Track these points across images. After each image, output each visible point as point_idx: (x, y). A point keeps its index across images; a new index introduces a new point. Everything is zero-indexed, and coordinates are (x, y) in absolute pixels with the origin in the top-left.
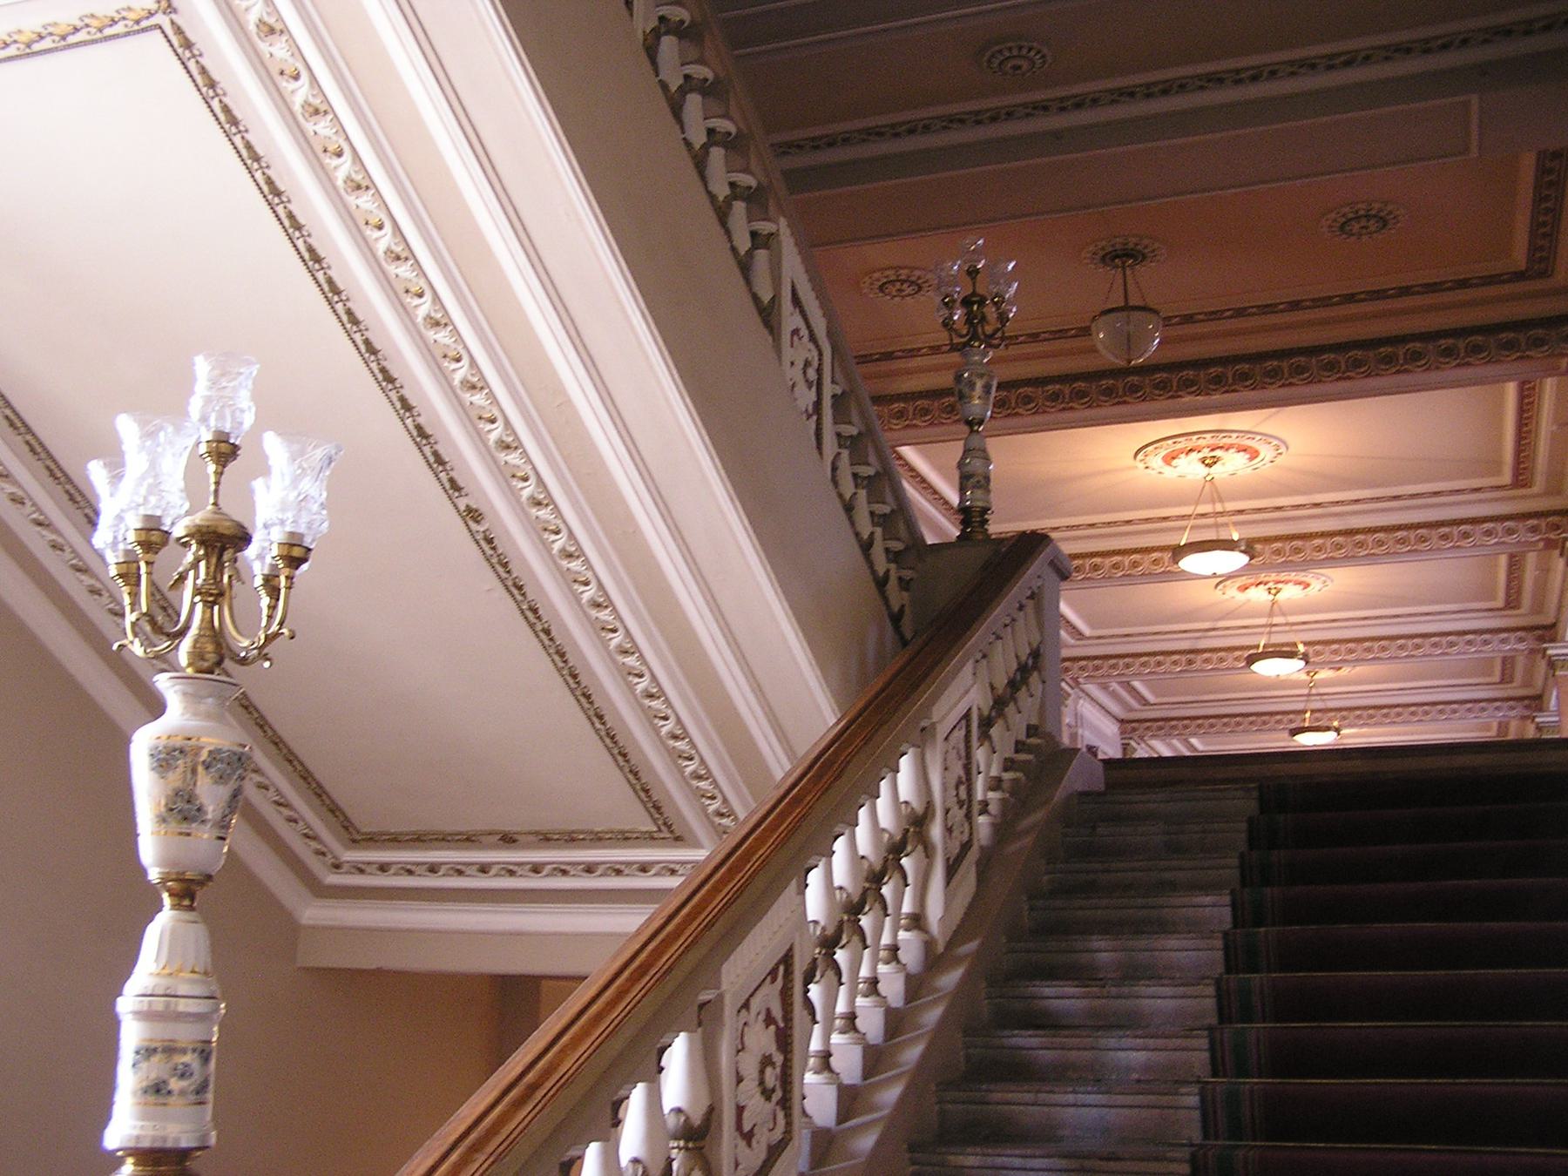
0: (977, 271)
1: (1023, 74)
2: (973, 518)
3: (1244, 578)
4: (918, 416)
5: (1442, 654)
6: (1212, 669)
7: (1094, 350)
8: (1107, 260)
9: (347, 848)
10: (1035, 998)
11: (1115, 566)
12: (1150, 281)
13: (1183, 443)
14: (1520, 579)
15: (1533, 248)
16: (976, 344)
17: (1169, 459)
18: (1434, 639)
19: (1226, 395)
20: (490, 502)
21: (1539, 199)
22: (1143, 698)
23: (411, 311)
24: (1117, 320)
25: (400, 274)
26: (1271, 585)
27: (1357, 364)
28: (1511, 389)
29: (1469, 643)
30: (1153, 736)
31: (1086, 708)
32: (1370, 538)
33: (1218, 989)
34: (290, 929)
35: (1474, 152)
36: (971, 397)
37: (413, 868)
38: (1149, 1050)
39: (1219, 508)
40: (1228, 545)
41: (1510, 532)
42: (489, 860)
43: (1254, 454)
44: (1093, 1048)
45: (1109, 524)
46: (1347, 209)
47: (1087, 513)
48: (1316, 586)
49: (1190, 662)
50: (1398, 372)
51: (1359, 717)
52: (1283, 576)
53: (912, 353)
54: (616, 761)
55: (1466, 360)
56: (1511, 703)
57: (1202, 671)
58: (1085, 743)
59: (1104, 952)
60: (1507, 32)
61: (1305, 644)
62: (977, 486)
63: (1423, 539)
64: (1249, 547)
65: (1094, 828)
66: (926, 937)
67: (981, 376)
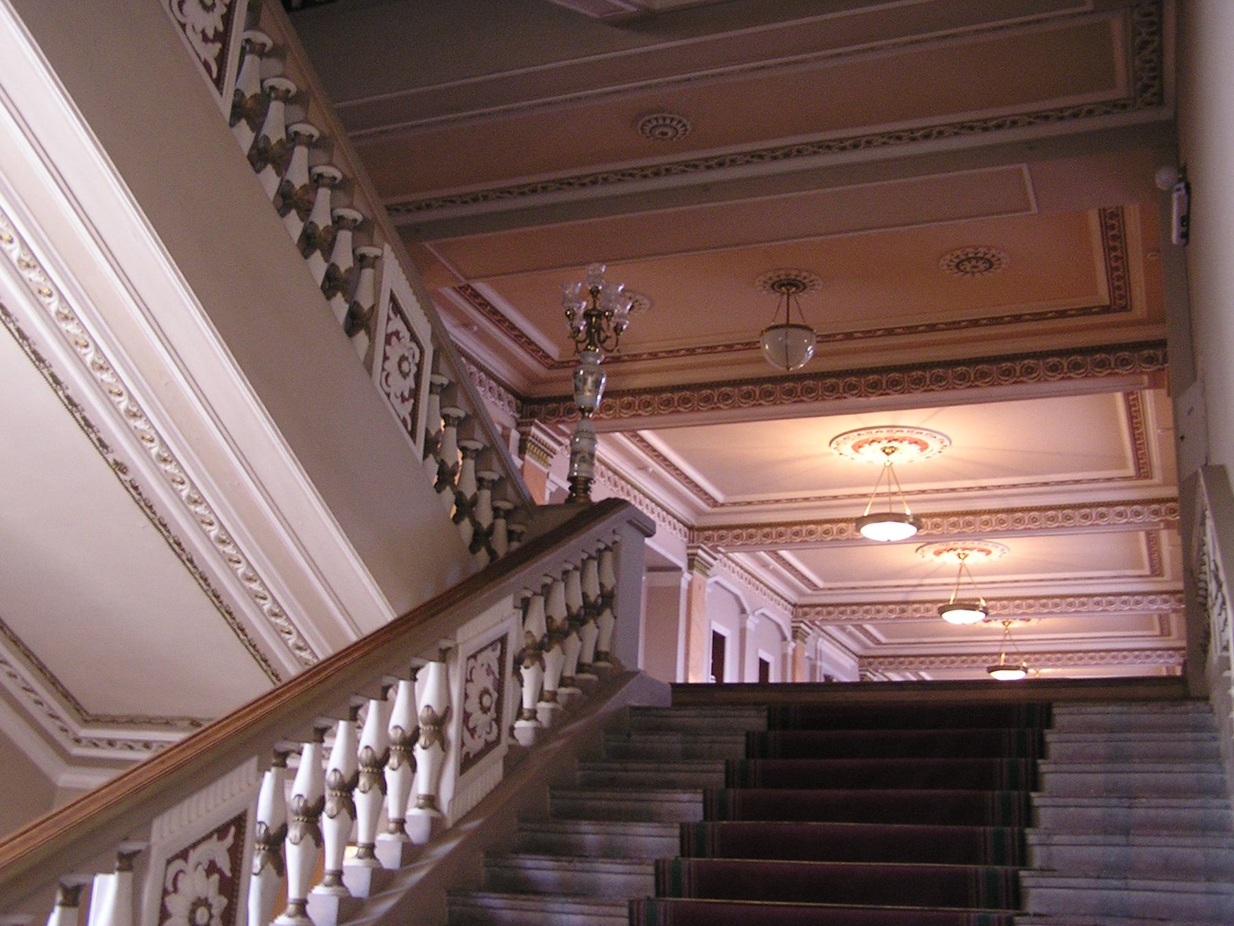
0: (598, 291)
1: (671, 139)
2: (580, 485)
3: (937, 545)
4: (642, 407)
5: (1102, 611)
6: (920, 617)
7: (761, 360)
8: (775, 286)
9: (82, 726)
10: (519, 868)
11: (826, 532)
12: (810, 306)
13: (865, 436)
14: (1159, 551)
15: (1113, 289)
16: (592, 348)
17: (857, 447)
18: (1096, 599)
19: (882, 398)
20: (131, 459)
21: (1108, 250)
22: (875, 638)
23: (46, 307)
24: (779, 335)
25: (33, 279)
26: (959, 551)
27: (983, 375)
28: (1119, 397)
29: (1124, 602)
30: (887, 669)
31: (825, 646)
32: (1026, 516)
33: (657, 869)
34: (50, 790)
35: (1034, 205)
36: (584, 391)
37: (133, 744)
38: (584, 914)
39: (894, 488)
40: (900, 518)
41: (1137, 514)
42: (117, 737)
43: (924, 446)
44: (543, 911)
45: (820, 498)
46: (958, 252)
47: (802, 489)
48: (996, 555)
49: (903, 611)
50: (1015, 383)
51: (1048, 660)
52: (969, 544)
53: (635, 358)
54: (260, 665)
55: (1068, 375)
56: (1171, 652)
57: (913, 618)
58: (823, 672)
59: (590, 834)
60: (1045, 117)
61: (986, 600)
62: (583, 460)
63: (1068, 518)
64: (917, 521)
65: (629, 735)
66: (435, 814)
67: (592, 374)
